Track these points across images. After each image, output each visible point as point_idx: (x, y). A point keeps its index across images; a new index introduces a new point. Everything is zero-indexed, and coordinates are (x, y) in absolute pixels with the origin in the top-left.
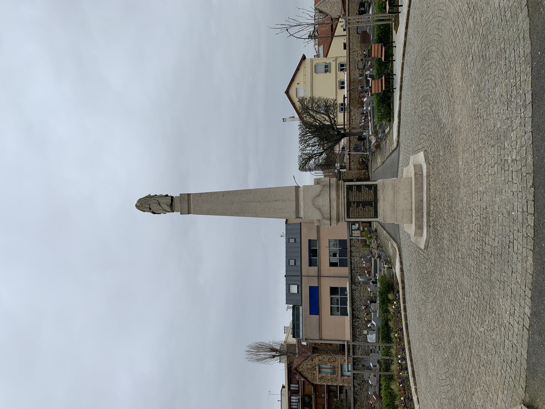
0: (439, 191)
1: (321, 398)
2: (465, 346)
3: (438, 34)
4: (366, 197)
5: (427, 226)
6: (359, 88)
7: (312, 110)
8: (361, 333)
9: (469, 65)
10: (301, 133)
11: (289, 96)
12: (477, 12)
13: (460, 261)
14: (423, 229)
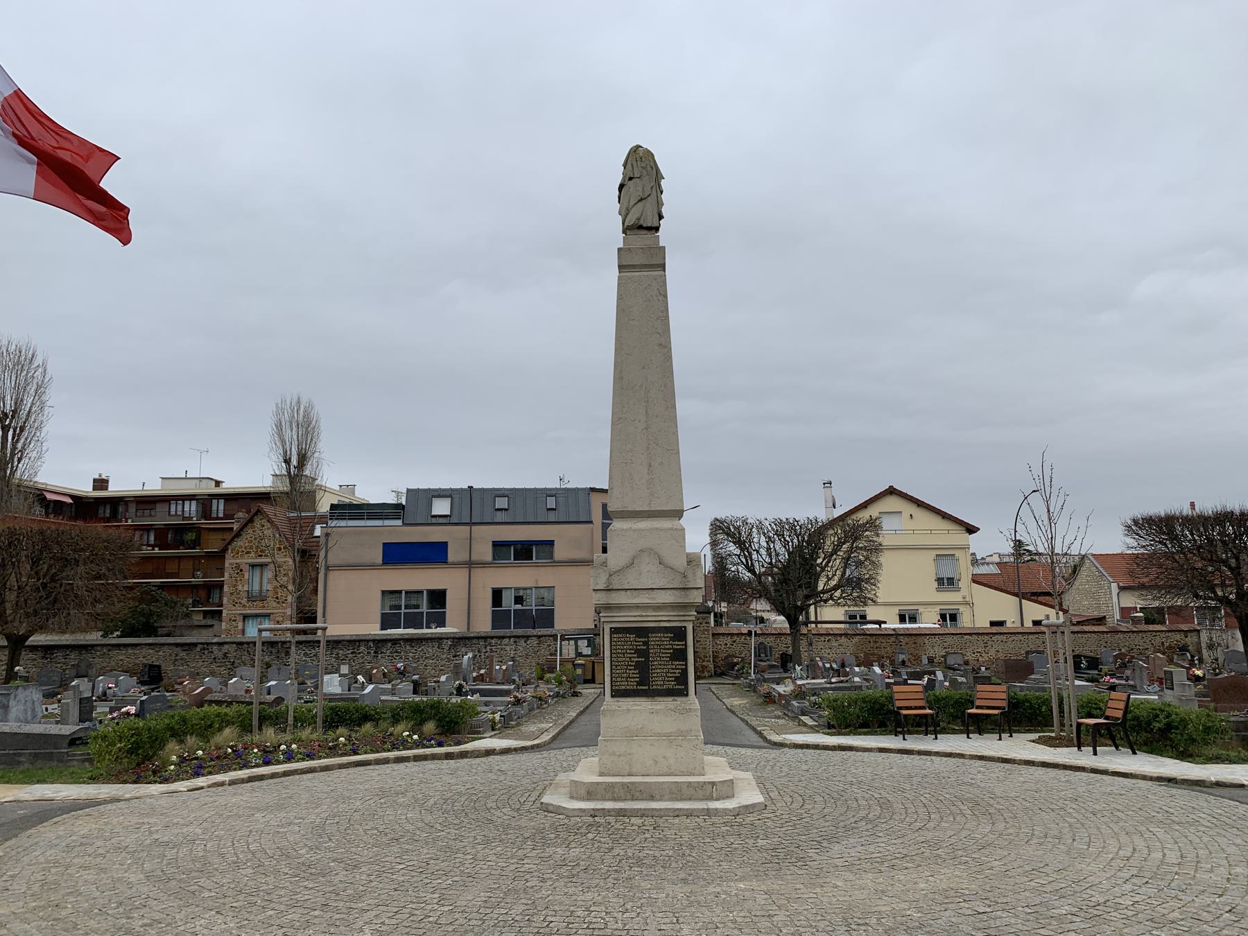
0: (675, 836)
1: (194, 570)
2: (328, 894)
3: (1033, 835)
4: (659, 671)
5: (593, 810)
6: (902, 657)
7: (852, 548)
8: (342, 660)
9: (967, 906)
10: (798, 524)
11: (884, 496)
12: (1087, 923)
13: (520, 884)
14: (588, 800)
